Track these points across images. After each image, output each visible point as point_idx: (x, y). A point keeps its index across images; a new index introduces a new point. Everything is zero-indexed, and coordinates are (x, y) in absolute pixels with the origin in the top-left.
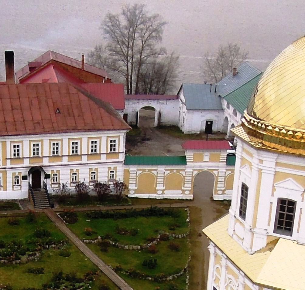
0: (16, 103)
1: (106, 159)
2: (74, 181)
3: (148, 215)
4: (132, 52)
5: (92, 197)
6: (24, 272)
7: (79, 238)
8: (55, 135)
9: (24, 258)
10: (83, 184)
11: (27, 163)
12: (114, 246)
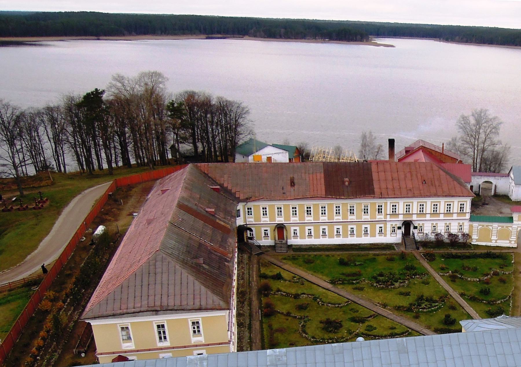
0: (395, 175)
2: (434, 231)
3: (485, 257)
6: (397, 294)
7: (436, 272)
8: (422, 199)
9: (397, 285)
10: (440, 234)
11: (401, 218)
12: (460, 278)
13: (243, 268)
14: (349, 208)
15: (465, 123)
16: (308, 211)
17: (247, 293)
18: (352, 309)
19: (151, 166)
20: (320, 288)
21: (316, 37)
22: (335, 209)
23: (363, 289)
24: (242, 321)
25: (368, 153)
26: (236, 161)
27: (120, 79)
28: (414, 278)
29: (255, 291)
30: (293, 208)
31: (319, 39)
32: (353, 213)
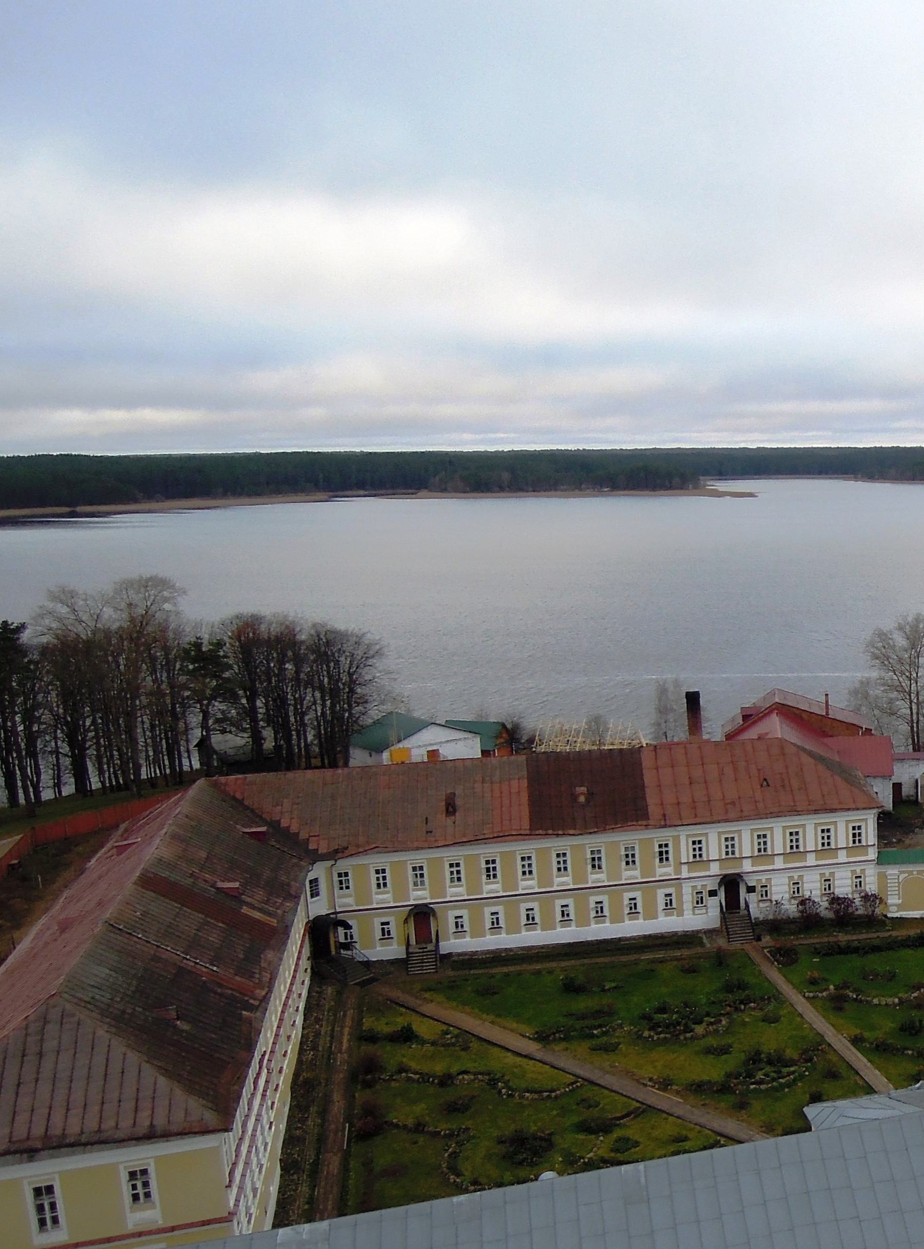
0: (697, 773)
1: (752, 866)
2: (796, 895)
3: (916, 946)
4: (917, 686)
5: (827, 920)
6: (697, 1053)
7: (797, 990)
8: (759, 821)
9: (699, 1029)
10: (810, 900)
11: (715, 869)
12: (856, 1000)
13: (318, 1020)
14: (589, 856)
15: (884, 647)
16: (488, 870)
17: (320, 1083)
18: (583, 1100)
19: (135, 790)
20: (509, 1054)
21: (581, 484)
22: (554, 860)
23: (616, 1048)
24: (296, 1156)
25: (672, 725)
26: (352, 763)
27: (66, 596)
28: (741, 1011)
29: (341, 1075)
30: (451, 865)
31: (588, 488)
32: (600, 868)
